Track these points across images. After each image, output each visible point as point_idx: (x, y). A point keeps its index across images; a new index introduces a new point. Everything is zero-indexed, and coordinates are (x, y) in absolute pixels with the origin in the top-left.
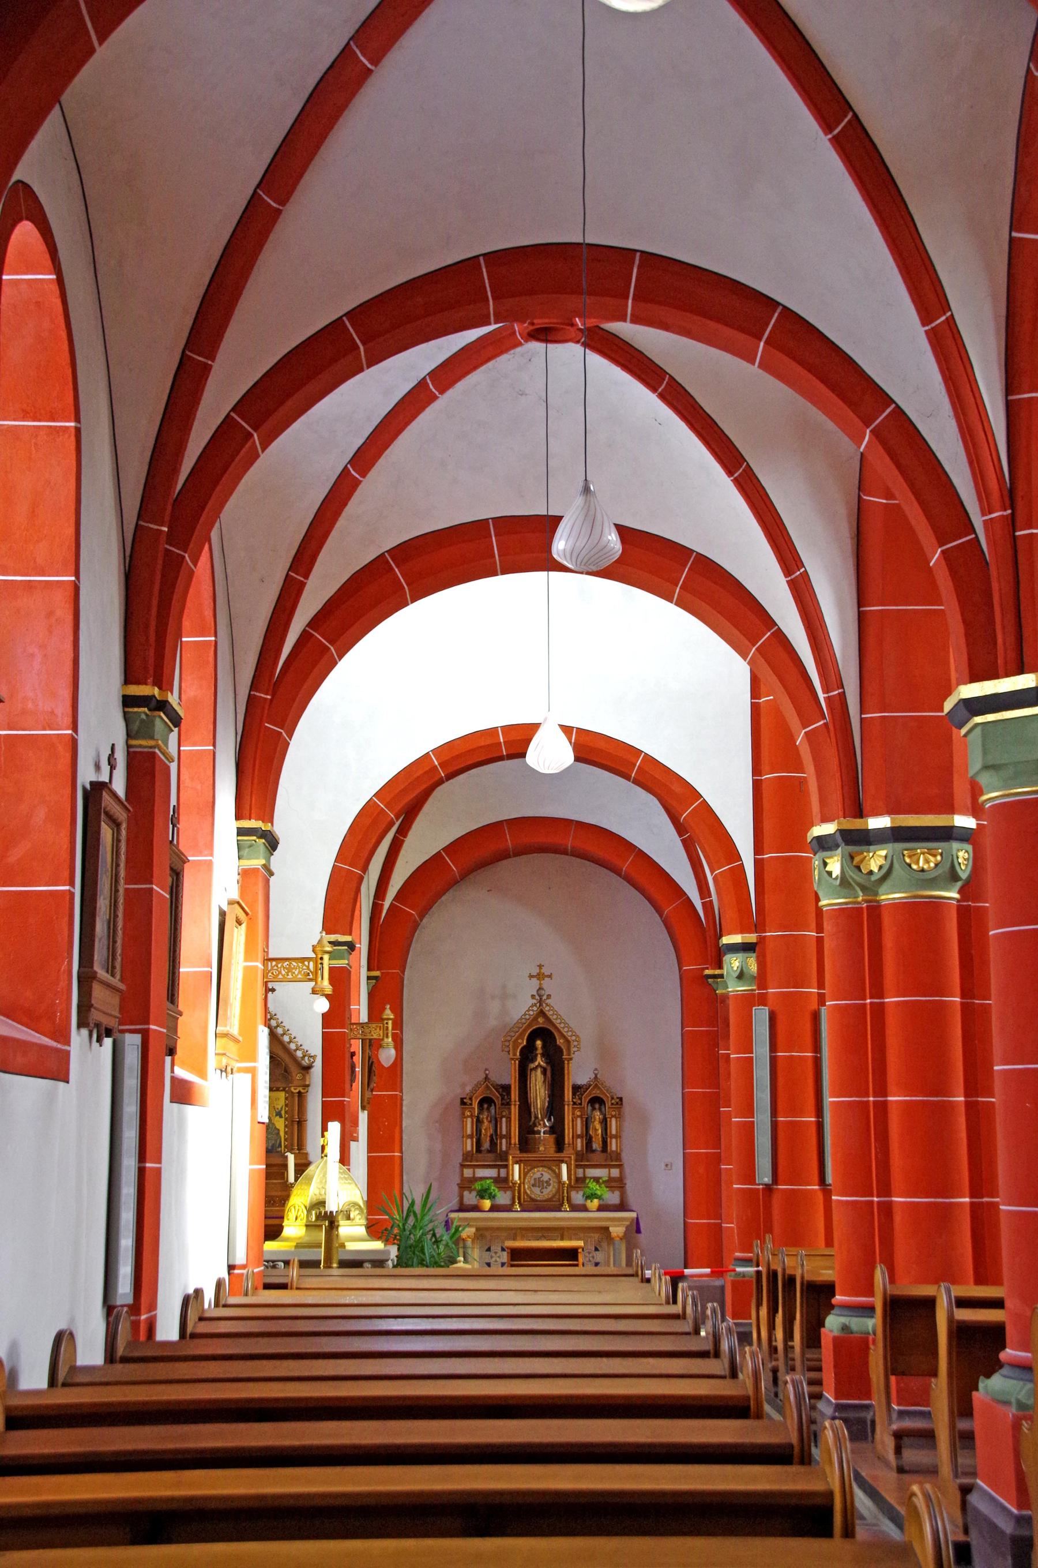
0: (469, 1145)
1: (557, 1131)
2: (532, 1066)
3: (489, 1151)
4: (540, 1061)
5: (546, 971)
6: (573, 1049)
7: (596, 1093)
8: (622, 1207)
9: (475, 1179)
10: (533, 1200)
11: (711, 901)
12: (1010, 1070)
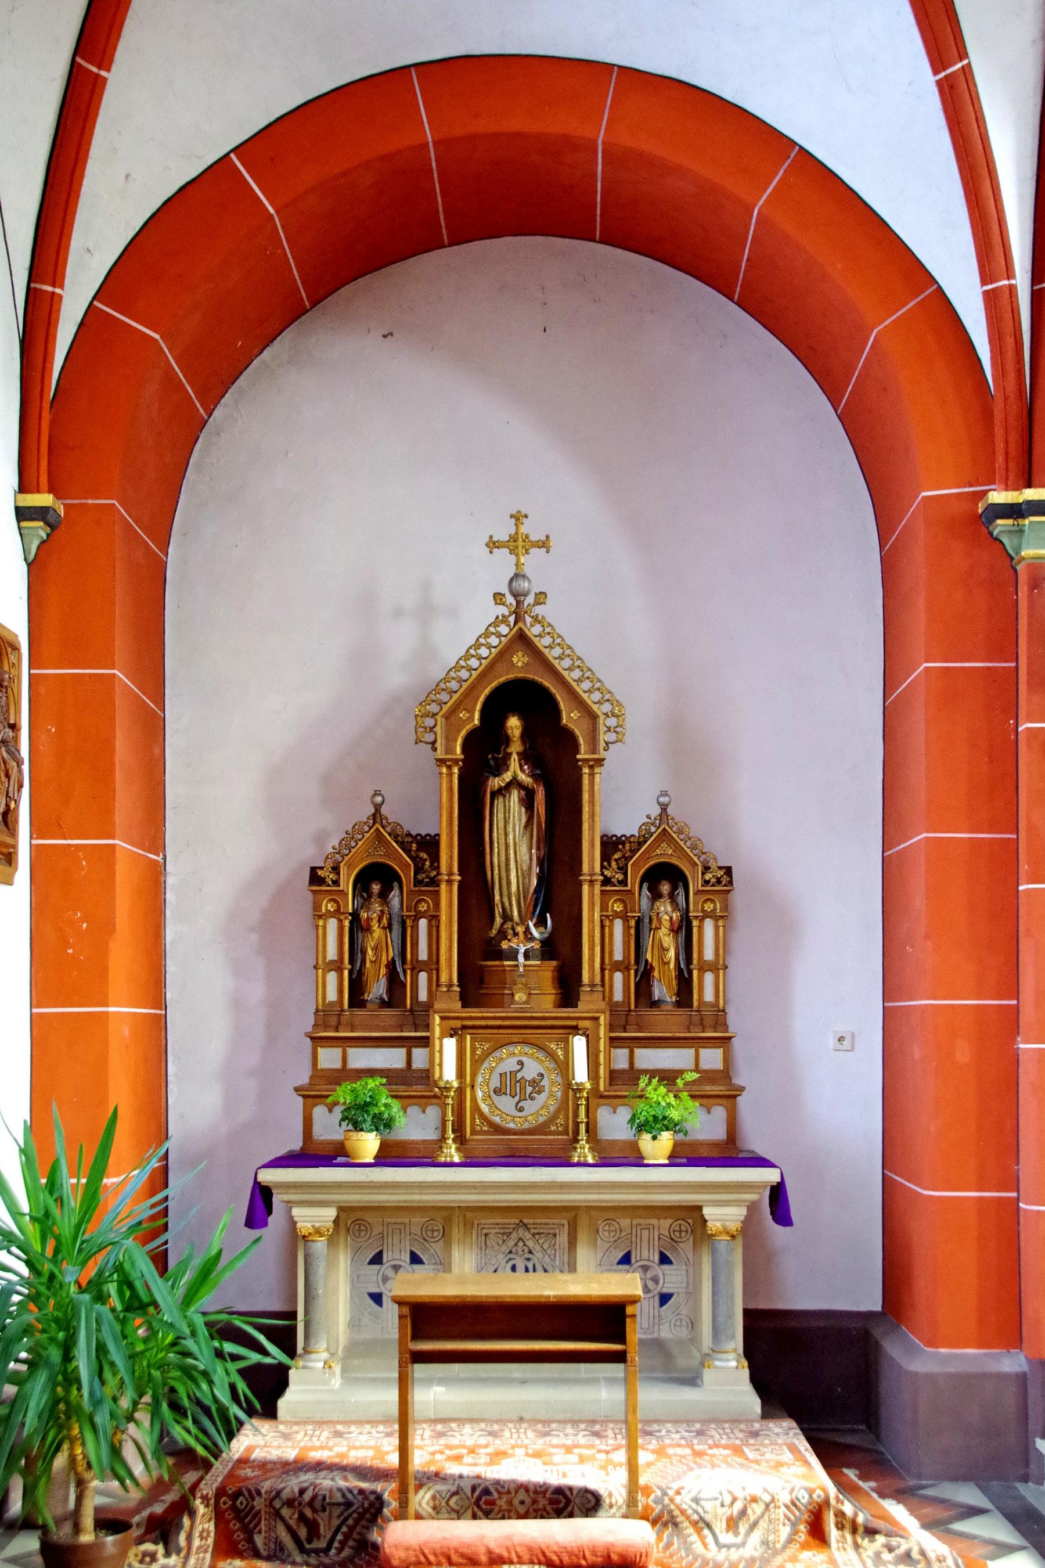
0: (333, 988)
1: (562, 952)
2: (496, 782)
3: (384, 1004)
4: (516, 770)
5: (532, 529)
6: (603, 737)
7: (665, 854)
8: (729, 1153)
10: (497, 1129)
11: (1012, 290)
12: (897, 1001)
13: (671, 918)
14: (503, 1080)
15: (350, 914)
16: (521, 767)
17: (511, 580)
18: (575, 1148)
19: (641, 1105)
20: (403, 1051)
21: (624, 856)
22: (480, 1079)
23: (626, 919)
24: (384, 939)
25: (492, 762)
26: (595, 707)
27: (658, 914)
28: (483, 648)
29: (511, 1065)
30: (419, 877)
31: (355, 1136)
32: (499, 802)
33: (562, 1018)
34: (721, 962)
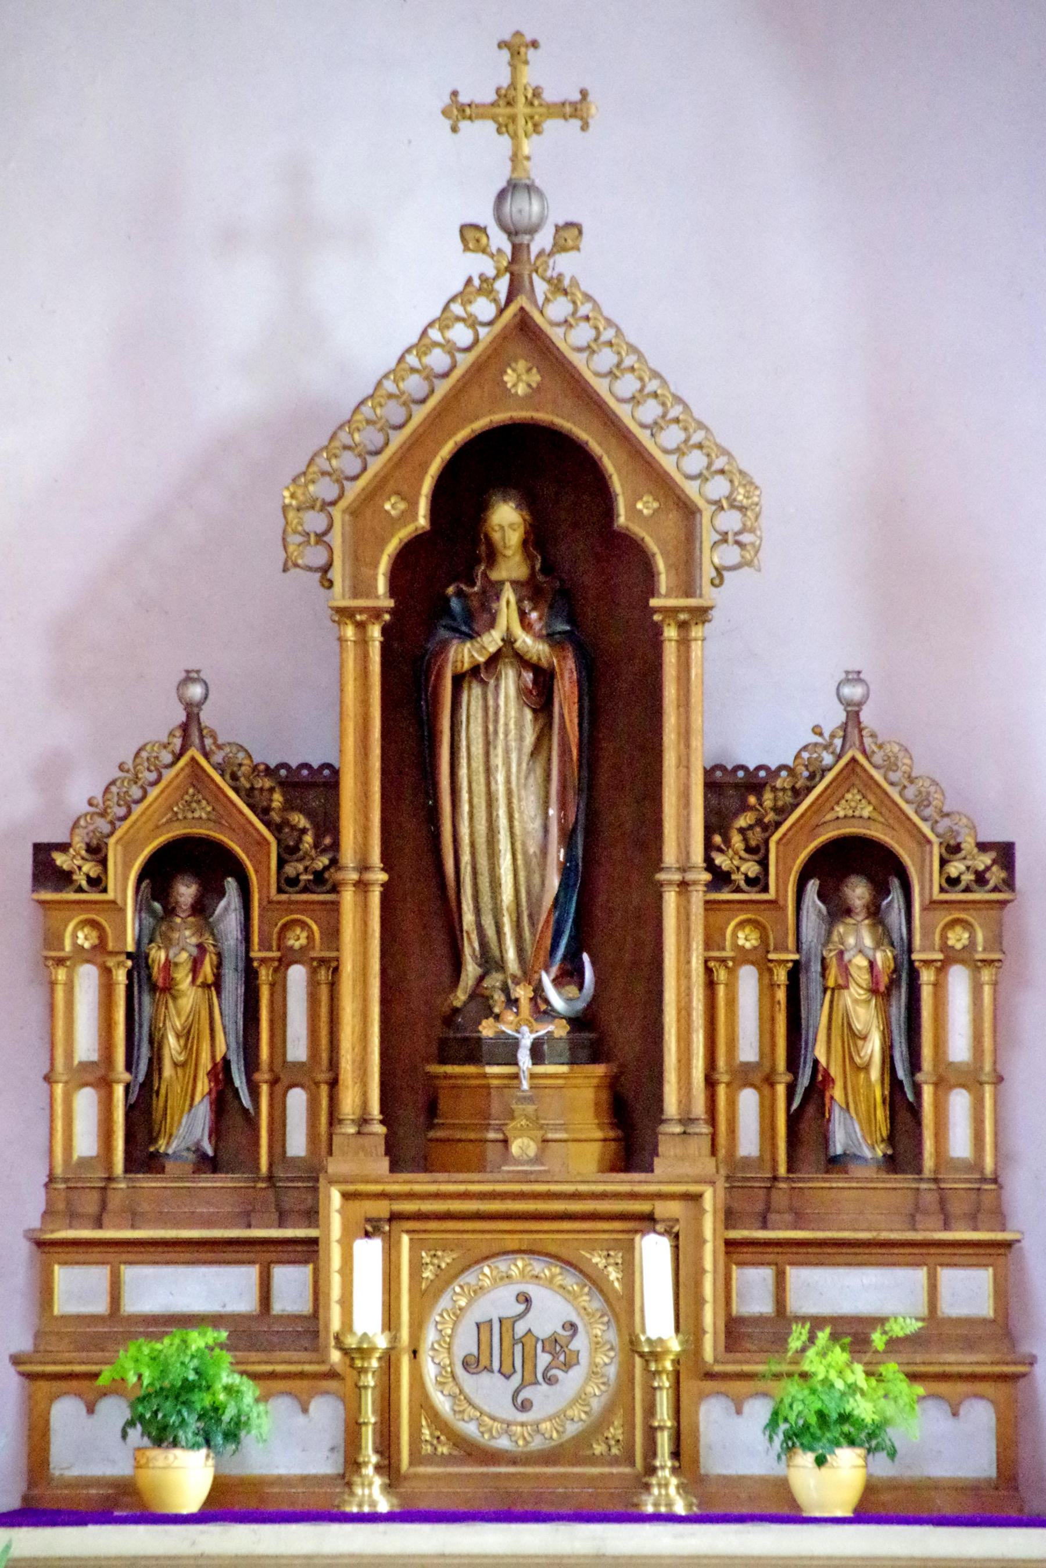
0: (87, 1126)
1: (617, 1044)
2: (464, 654)
4: (512, 623)
5: (549, 75)
6: (710, 558)
7: (854, 816)
9: (116, 1327)
10: (471, 1452)
13: (872, 964)
14: (485, 1338)
15: (129, 956)
16: (523, 615)
17: (501, 196)
18: (647, 1487)
19: (793, 1389)
20: (250, 1274)
21: (759, 822)
22: (431, 1336)
23: (765, 967)
24: (205, 1014)
25: (455, 604)
26: (691, 489)
27: (841, 953)
28: (437, 352)
29: (500, 1302)
30: (290, 870)
31: (162, 1457)
32: (473, 696)
33: (437, 1196)
34: (988, 1067)
